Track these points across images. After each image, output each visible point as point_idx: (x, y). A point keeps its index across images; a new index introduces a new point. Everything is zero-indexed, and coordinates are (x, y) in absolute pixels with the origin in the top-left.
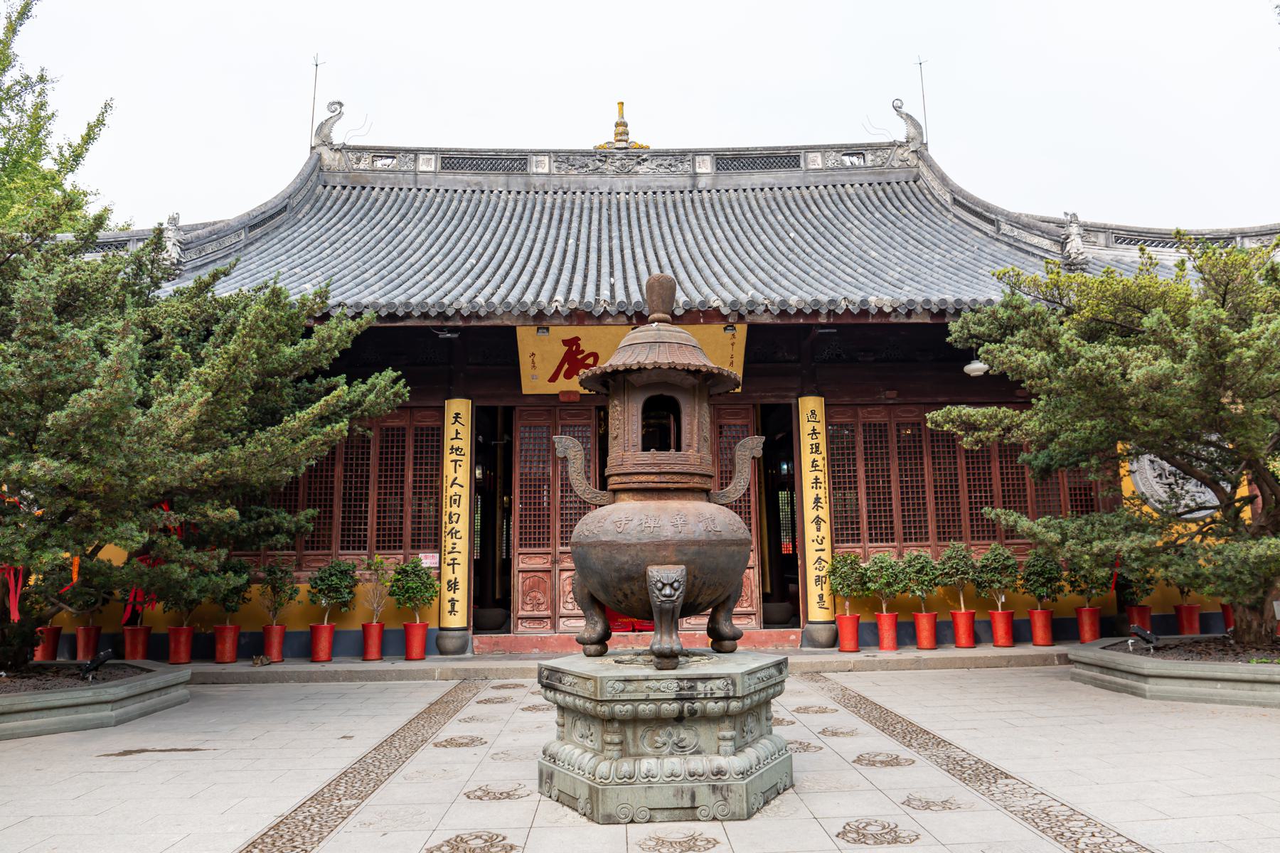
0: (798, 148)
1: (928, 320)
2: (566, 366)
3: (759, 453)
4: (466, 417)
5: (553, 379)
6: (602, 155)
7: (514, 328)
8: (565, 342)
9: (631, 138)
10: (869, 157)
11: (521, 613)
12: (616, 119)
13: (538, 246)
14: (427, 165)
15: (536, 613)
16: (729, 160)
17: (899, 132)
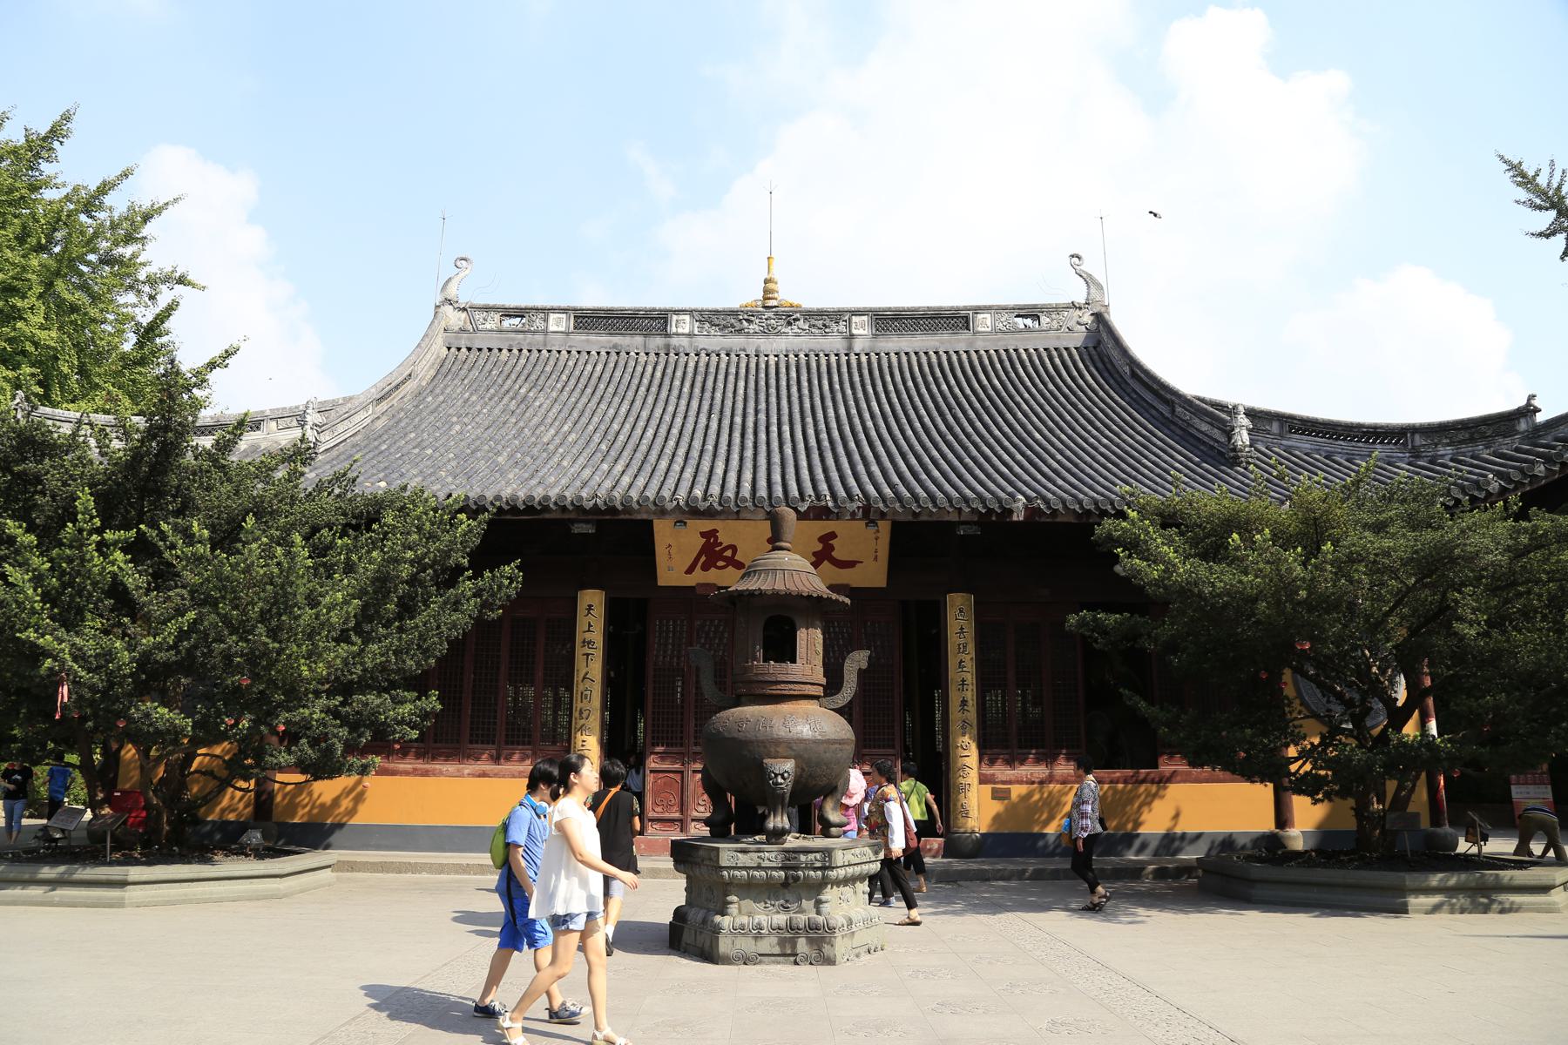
0: (966, 308)
1: (1073, 520)
2: (703, 558)
3: (864, 665)
4: (599, 612)
5: (690, 571)
6: (748, 315)
7: (651, 522)
8: (703, 534)
10: (1044, 319)
12: (766, 276)
13: (679, 420)
14: (557, 323)
15: (667, 815)
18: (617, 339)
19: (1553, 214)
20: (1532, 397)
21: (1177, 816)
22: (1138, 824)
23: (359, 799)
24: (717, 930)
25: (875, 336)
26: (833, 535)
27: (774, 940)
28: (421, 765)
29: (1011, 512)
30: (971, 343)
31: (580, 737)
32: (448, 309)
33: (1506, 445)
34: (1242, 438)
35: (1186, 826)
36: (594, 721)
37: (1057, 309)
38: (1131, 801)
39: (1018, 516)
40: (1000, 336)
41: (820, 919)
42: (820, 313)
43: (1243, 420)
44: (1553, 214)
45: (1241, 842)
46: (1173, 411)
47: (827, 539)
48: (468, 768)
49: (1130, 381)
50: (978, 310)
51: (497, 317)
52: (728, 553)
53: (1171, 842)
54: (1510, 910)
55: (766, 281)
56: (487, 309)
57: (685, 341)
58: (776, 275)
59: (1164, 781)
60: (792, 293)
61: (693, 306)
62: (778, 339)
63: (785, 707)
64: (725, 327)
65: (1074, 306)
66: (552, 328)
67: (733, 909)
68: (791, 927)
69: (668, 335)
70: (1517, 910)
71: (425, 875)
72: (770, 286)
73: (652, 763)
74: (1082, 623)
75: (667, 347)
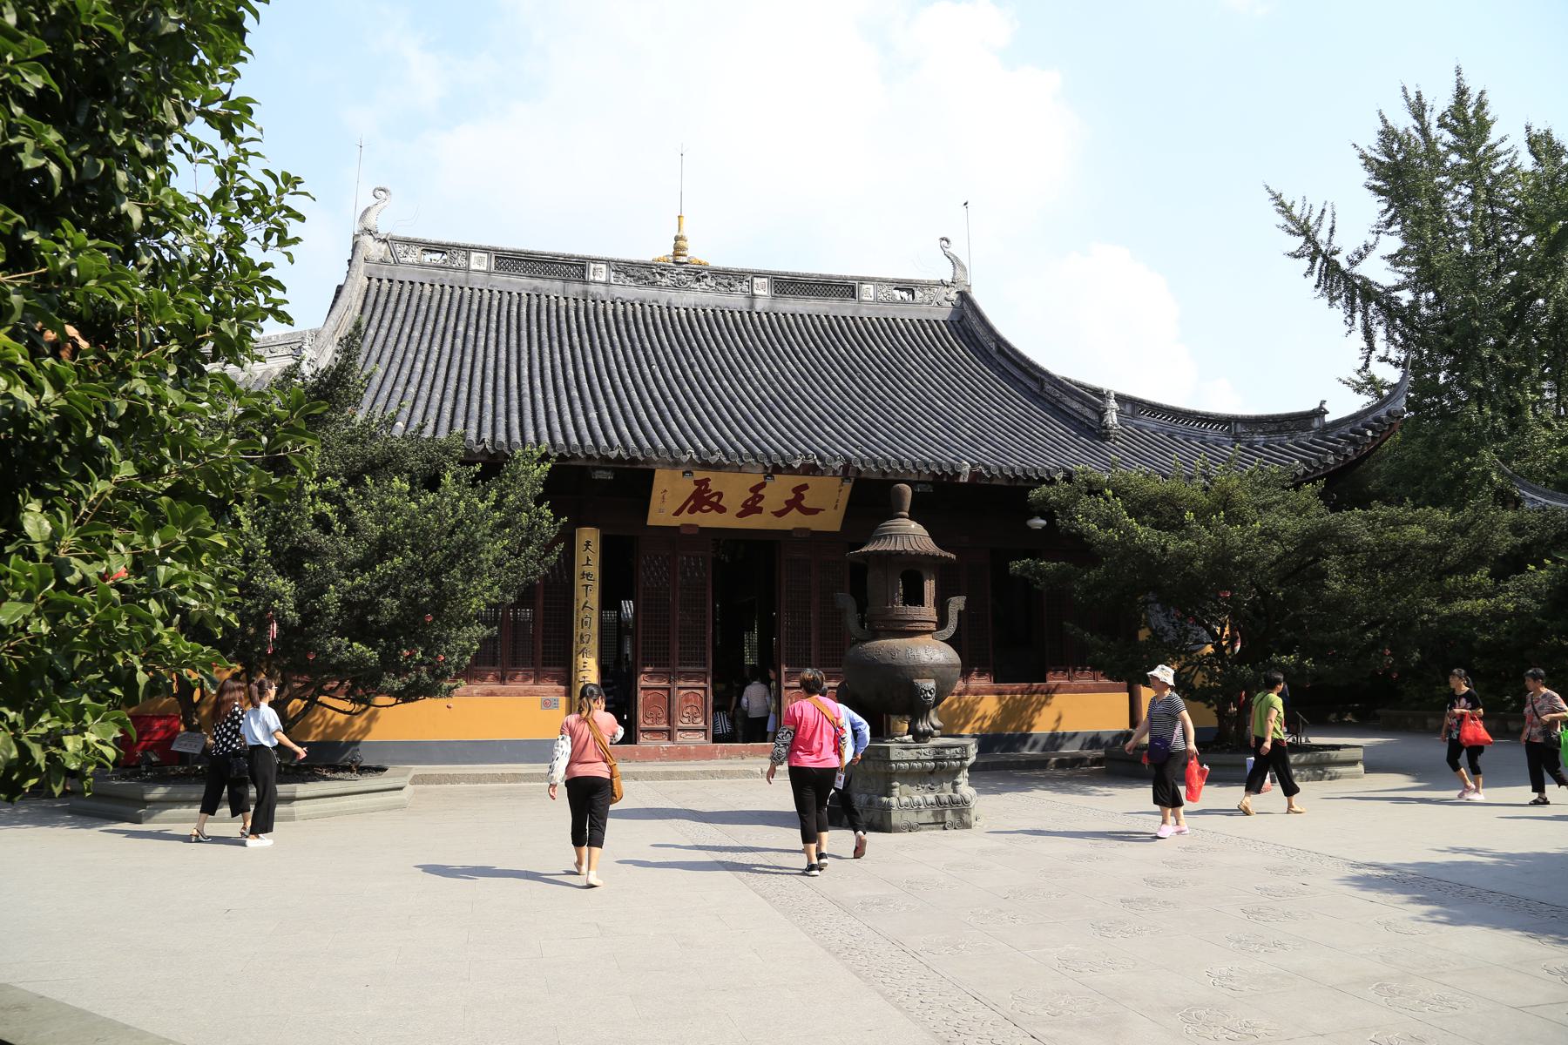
0: (852, 278)
4: (596, 546)
5: (677, 513)
9: (689, 253)
10: (918, 294)
11: (643, 726)
12: (676, 233)
14: (479, 262)
15: (656, 726)
18: (537, 282)
19: (1303, 239)
20: (1323, 402)
21: (1059, 719)
22: (1031, 726)
24: (889, 807)
25: (774, 297)
26: (805, 487)
27: (930, 813)
29: (959, 474)
30: (857, 311)
33: (1304, 437)
34: (1112, 418)
35: (1066, 728)
36: (593, 644)
38: (1026, 708)
39: (964, 479)
41: (958, 796)
42: (726, 273)
43: (1113, 404)
44: (1303, 239)
45: (1105, 738)
46: (1042, 388)
47: (799, 490)
48: (477, 688)
49: (997, 356)
50: (863, 280)
51: (418, 251)
52: (715, 499)
53: (1055, 740)
55: (677, 239)
56: (408, 242)
57: (601, 289)
58: (685, 232)
59: (1050, 692)
60: (701, 251)
61: (610, 256)
62: (688, 293)
63: (919, 639)
66: (473, 267)
67: (896, 792)
68: (939, 802)
69: (586, 282)
71: (463, 785)
72: (681, 243)
73: (642, 681)
74: (1026, 568)
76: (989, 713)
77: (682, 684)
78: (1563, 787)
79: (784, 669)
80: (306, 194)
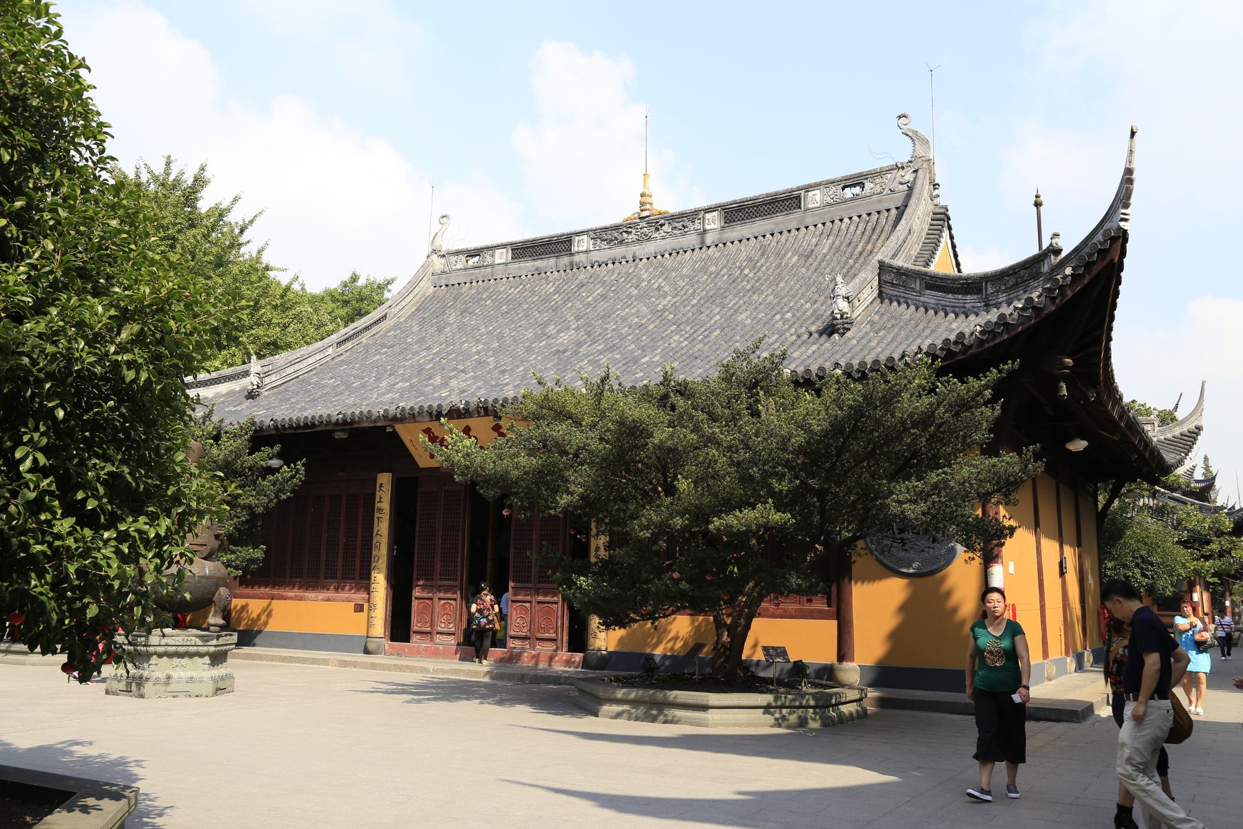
0: (799, 189)
10: (868, 185)
11: (415, 628)
14: (502, 256)
15: (424, 629)
16: (736, 213)
17: (902, 152)
18: (538, 263)
23: (269, 615)
28: (300, 593)
31: (373, 574)
32: (434, 257)
37: (880, 173)
40: (827, 209)
42: (681, 216)
48: (322, 595)
50: (808, 188)
54: (671, 722)
55: (642, 195)
56: (457, 253)
64: (611, 240)
65: (898, 168)
69: (572, 255)
70: (677, 722)
73: (417, 593)
75: (572, 264)
76: (681, 634)
77: (442, 595)
78: (1113, 825)
79: (511, 584)
80: (259, 252)
